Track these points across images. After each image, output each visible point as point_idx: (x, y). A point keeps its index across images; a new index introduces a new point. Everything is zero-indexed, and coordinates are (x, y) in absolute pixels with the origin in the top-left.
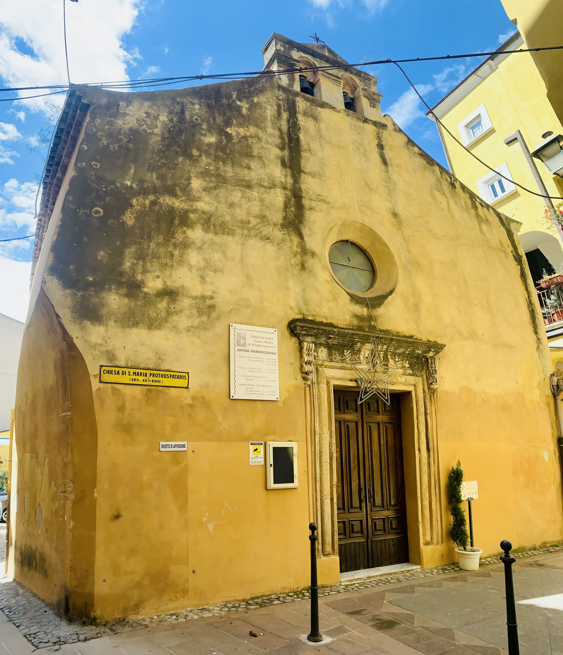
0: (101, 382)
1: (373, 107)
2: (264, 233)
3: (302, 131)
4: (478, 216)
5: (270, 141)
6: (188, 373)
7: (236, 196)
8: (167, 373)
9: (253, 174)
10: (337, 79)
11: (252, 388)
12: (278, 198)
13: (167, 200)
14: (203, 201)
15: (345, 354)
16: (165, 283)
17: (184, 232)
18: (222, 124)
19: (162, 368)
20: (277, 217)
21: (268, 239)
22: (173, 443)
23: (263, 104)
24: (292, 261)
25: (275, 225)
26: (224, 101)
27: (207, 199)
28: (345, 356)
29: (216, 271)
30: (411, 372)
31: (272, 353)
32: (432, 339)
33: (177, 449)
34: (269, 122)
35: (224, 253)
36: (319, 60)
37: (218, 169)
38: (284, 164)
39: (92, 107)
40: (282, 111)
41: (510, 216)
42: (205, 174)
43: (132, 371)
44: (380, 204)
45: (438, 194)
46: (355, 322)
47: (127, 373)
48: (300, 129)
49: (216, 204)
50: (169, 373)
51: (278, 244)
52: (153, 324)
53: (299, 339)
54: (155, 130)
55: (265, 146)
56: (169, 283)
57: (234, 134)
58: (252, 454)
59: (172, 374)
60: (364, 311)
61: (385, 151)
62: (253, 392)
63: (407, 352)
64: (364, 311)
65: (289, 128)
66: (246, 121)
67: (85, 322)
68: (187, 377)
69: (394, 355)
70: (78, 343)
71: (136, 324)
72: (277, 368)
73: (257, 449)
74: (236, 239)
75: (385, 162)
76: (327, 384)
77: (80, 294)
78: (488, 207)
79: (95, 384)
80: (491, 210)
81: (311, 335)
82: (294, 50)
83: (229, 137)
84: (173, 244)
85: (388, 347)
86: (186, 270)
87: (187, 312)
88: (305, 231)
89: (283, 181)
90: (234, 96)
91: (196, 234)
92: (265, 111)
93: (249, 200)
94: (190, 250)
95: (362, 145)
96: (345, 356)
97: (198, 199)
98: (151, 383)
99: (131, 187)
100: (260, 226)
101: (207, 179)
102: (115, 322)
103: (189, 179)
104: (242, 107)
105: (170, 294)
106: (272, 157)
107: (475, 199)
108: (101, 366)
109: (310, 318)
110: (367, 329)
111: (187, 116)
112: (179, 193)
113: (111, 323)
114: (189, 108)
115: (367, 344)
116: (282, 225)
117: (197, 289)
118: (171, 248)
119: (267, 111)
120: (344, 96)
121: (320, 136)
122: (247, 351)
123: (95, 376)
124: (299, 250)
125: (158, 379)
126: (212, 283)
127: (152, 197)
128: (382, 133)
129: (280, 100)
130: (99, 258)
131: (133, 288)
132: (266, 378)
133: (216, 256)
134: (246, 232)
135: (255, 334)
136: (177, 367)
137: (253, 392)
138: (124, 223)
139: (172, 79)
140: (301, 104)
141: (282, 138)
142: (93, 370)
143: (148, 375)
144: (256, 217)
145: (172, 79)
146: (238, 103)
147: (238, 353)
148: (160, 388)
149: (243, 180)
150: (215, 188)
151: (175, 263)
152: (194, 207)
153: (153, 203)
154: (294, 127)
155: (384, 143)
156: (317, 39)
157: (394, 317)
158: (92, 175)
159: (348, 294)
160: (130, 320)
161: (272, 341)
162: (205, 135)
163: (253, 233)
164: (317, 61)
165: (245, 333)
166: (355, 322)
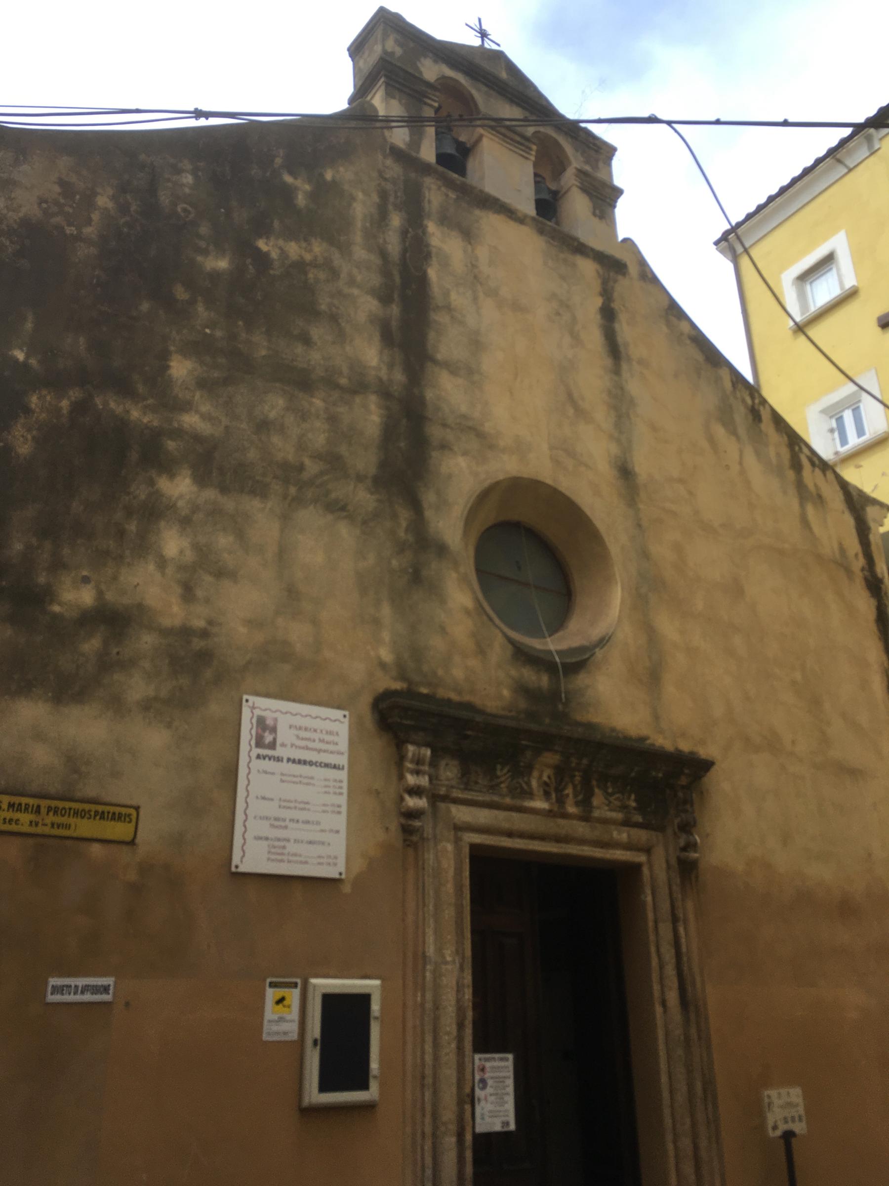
2: (333, 495)
3: (434, 261)
4: (800, 485)
5: (359, 278)
6: (137, 809)
7: (274, 405)
8: (87, 807)
9: (315, 356)
10: (523, 141)
11: (284, 847)
12: (370, 416)
13: (112, 404)
14: (197, 412)
15: (499, 773)
16: (100, 594)
17: (151, 483)
19: (79, 795)
20: (366, 461)
21: (343, 508)
22: (81, 982)
23: (346, 187)
25: (360, 478)
26: (255, 171)
28: (498, 777)
32: (685, 746)
33: (88, 997)
35: (240, 535)
38: (387, 338)
40: (390, 207)
41: (867, 489)
44: (597, 448)
45: (720, 431)
46: (522, 704)
49: (225, 421)
50: (93, 807)
52: (68, 690)
54: (88, 231)
55: (346, 290)
56: (109, 596)
57: (274, 255)
58: (270, 1012)
59: (100, 808)
60: (545, 681)
61: (617, 326)
62: (285, 858)
63: (633, 774)
66: (305, 226)
72: (343, 800)
74: (269, 504)
75: (614, 349)
76: (458, 991)
78: (824, 466)
80: (830, 475)
82: (426, 57)
83: (263, 259)
86: (151, 567)
87: (147, 664)
88: (429, 498)
90: (278, 161)
91: (180, 487)
93: (304, 416)
94: (162, 524)
95: (568, 307)
96: (498, 777)
97: (186, 406)
98: (47, 830)
99: (25, 364)
100: (325, 478)
103: (164, 356)
105: (114, 620)
106: (361, 317)
107: (800, 448)
109: (424, 690)
111: (164, 198)
112: (141, 388)
114: (169, 180)
117: (174, 613)
118: (119, 516)
120: (536, 183)
121: (475, 277)
122: (279, 759)
125: (64, 820)
126: (207, 601)
127: (75, 394)
128: (615, 281)
129: (386, 179)
132: (318, 823)
133: (224, 540)
134: (293, 490)
135: (299, 721)
137: (285, 858)
139: (138, 111)
140: (435, 195)
141: (386, 273)
143: (43, 810)
144: (317, 456)
145: (138, 111)
146: (288, 179)
147: (257, 764)
151: (128, 553)
153: (81, 407)
154: (417, 251)
155: (616, 305)
156: (483, 35)
157: (613, 702)
159: (510, 641)
162: (205, 252)
164: (479, 90)
165: (276, 720)
166: (522, 704)
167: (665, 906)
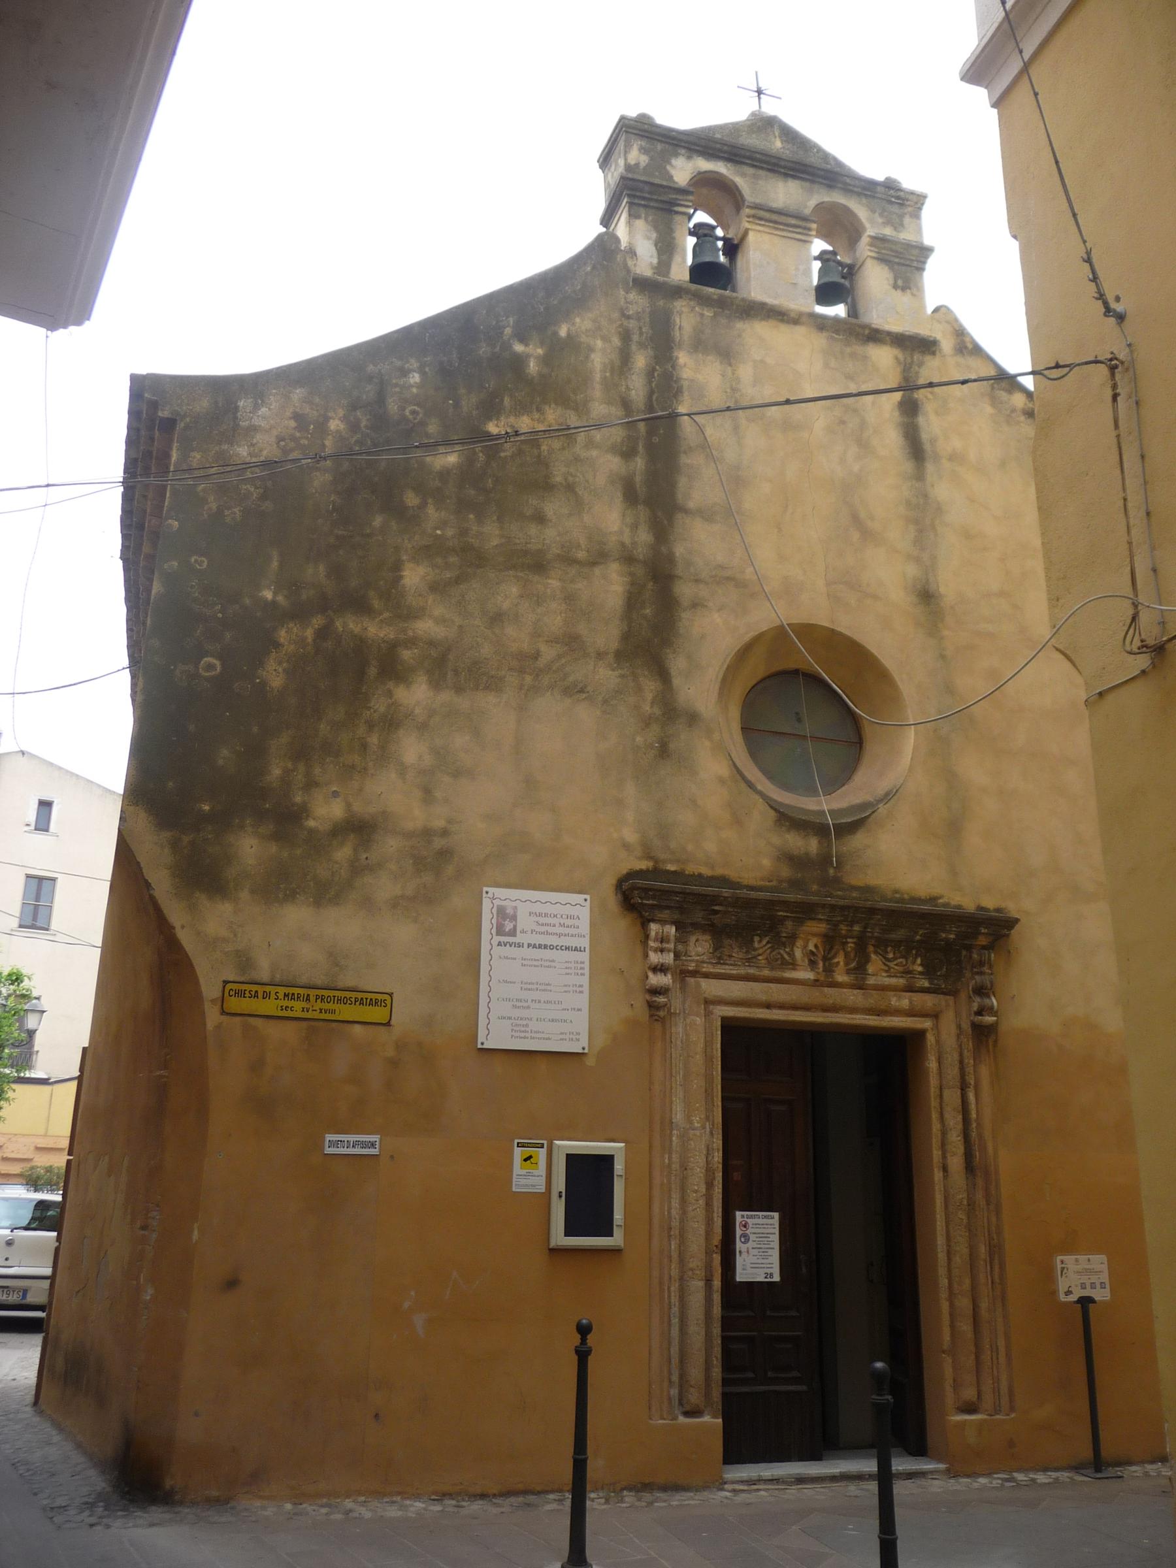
0: (223, 1012)
1: (903, 289)
2: (571, 679)
6: (391, 995)
8: (348, 995)
9: (550, 533)
11: (527, 1025)
12: (610, 587)
13: (350, 624)
15: (756, 945)
16: (348, 805)
17: (390, 694)
18: (474, 412)
19: (341, 985)
20: (606, 635)
21: (582, 691)
22: (352, 1138)
23: (583, 339)
24: (638, 739)
25: (600, 655)
27: (438, 611)
29: (457, 774)
30: (927, 984)
31: (576, 949)
34: (598, 386)
36: (751, 171)
37: (464, 532)
38: (631, 496)
39: (181, 425)
40: (634, 347)
42: (430, 551)
43: (282, 991)
46: (786, 872)
47: (273, 996)
48: (679, 391)
50: (354, 995)
51: (605, 702)
52: (325, 894)
53: (642, 916)
55: (584, 454)
56: (358, 807)
59: (360, 995)
60: (813, 845)
61: (921, 420)
64: (813, 845)
65: (651, 393)
67: (197, 894)
68: (388, 1002)
69: (882, 945)
70: (185, 938)
71: (291, 896)
72: (585, 981)
73: (530, 1157)
77: (186, 839)
79: (212, 1017)
81: (668, 907)
82: (676, 155)
84: (366, 722)
85: (865, 928)
86: (393, 775)
88: (677, 664)
89: (627, 541)
91: (416, 695)
92: (587, 357)
93: (539, 600)
94: (401, 732)
96: (755, 950)
98: (316, 1015)
99: (274, 602)
100: (563, 661)
101: (439, 560)
102: (252, 892)
103: (397, 567)
104: (528, 356)
105: (360, 829)
106: (601, 480)
108: (226, 982)
110: (815, 887)
111: (392, 406)
112: (376, 604)
113: (244, 895)
114: (396, 385)
115: (809, 923)
116: (619, 655)
117: (415, 816)
118: (361, 730)
119: (593, 356)
122: (520, 945)
123: (213, 1001)
124: (657, 711)
125: (331, 1006)
127: (318, 621)
129: (629, 317)
130: (221, 762)
131: (286, 820)
133: (460, 740)
134: (528, 679)
135: (538, 908)
136: (372, 982)
138: (264, 684)
140: (686, 318)
142: (210, 988)
143: (312, 999)
144: (553, 641)
146: (519, 348)
147: (497, 951)
148: (334, 1025)
149: (526, 553)
150: (458, 580)
151: (371, 764)
152: (410, 633)
153: (323, 633)
158: (192, 587)
160: (279, 886)
161: (576, 922)
163: (546, 680)
164: (743, 175)
166: (786, 872)
167: (952, 1072)
